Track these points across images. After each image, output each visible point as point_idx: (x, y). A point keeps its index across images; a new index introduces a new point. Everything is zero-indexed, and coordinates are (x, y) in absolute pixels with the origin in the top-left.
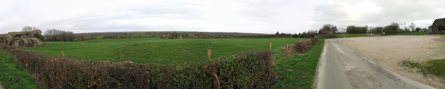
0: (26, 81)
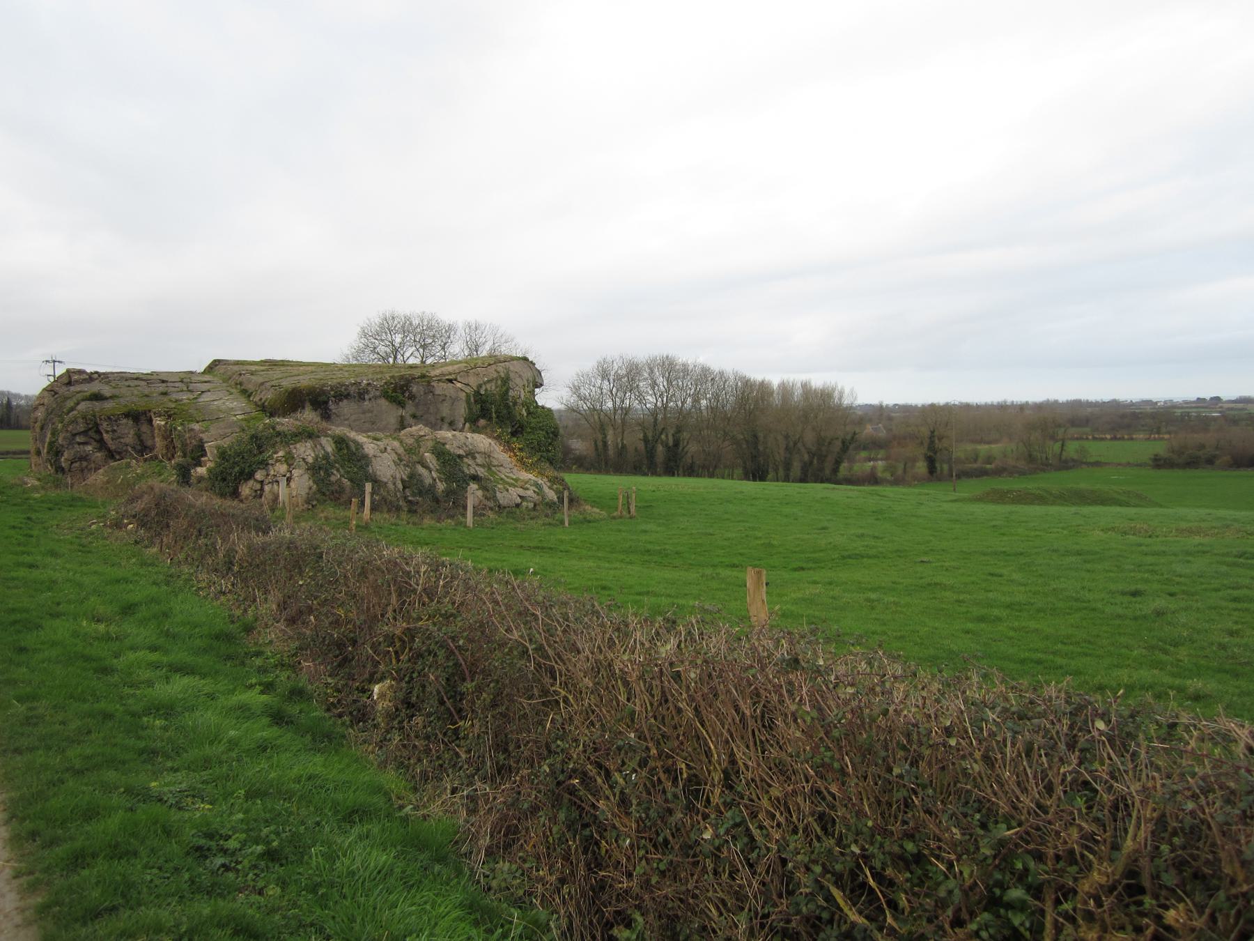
0: (364, 853)
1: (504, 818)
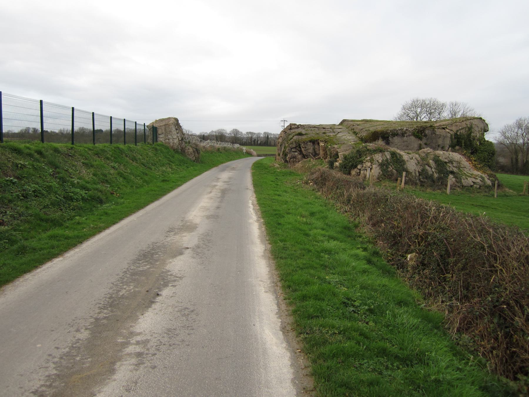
1: (465, 318)
